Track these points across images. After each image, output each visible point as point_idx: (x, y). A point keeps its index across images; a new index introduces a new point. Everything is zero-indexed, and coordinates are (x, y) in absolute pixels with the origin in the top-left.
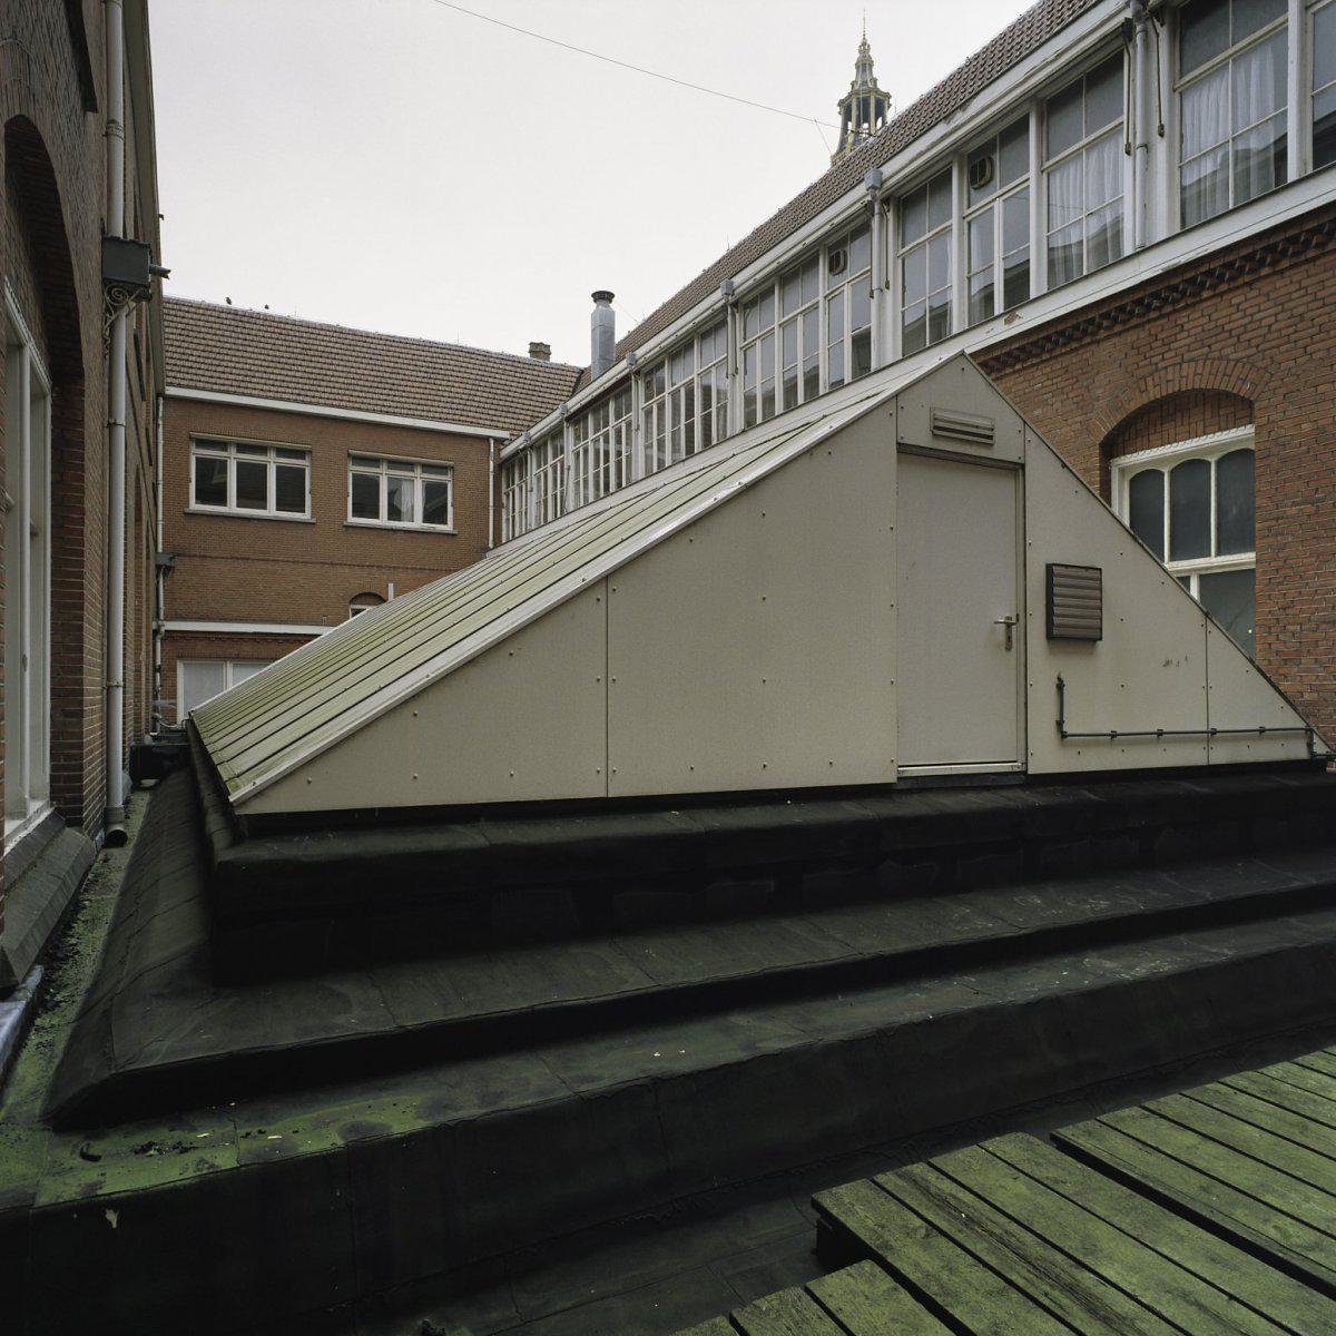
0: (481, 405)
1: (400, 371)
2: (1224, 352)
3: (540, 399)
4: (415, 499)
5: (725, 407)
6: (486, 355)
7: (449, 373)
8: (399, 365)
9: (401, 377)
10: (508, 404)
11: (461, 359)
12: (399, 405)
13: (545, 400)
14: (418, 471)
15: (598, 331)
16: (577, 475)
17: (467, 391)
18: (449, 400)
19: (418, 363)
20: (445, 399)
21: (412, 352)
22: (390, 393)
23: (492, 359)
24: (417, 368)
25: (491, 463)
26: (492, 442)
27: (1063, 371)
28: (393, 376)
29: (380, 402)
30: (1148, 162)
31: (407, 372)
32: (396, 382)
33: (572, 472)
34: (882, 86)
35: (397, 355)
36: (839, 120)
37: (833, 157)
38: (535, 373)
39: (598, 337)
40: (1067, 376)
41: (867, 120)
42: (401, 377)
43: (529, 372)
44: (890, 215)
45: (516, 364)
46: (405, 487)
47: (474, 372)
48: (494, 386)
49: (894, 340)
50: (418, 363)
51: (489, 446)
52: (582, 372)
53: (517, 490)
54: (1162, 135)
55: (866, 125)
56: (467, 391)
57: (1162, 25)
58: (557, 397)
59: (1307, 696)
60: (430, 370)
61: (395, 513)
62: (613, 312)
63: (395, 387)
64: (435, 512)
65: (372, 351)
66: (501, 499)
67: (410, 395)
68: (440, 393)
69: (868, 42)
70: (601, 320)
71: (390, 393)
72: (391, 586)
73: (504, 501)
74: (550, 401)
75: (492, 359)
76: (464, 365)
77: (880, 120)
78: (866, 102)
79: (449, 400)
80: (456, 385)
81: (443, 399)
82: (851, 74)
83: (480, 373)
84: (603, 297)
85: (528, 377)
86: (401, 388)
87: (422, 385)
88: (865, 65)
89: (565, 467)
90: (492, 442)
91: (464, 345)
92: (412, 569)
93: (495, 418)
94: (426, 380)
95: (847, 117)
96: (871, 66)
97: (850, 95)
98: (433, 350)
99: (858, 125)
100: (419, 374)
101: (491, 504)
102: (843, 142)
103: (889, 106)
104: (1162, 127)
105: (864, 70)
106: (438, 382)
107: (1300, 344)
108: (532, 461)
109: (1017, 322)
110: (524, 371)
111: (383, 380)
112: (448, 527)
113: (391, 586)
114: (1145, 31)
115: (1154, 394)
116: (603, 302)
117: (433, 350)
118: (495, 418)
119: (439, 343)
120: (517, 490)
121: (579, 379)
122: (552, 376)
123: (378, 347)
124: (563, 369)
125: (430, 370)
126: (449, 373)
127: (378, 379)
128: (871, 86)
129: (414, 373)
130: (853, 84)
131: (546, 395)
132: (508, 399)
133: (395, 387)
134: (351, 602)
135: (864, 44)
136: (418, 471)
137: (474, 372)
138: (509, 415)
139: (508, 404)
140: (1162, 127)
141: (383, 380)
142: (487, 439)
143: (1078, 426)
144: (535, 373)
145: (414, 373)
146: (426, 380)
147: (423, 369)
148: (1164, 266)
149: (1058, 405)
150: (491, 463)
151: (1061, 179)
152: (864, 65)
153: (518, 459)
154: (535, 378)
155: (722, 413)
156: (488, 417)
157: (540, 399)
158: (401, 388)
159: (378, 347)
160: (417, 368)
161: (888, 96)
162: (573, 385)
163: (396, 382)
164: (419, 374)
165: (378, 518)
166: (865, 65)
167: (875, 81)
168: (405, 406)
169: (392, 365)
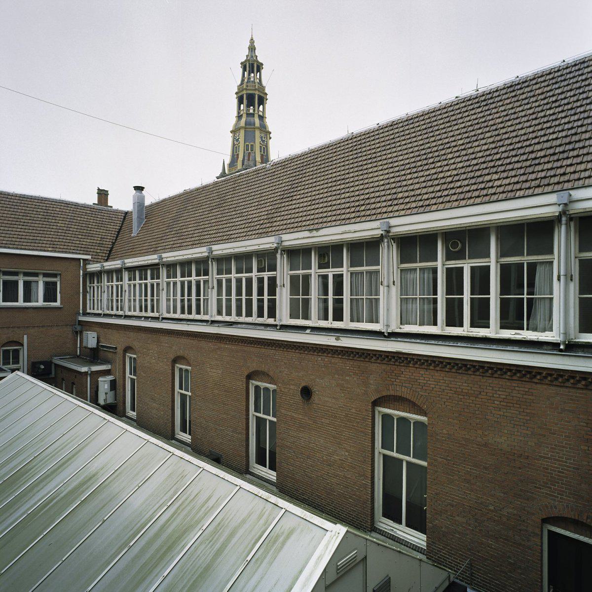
0: (74, 233)
1: (28, 215)
2: (417, 390)
3: (105, 228)
4: (40, 290)
5: (208, 299)
6: (76, 205)
7: (56, 215)
8: (27, 212)
9: (28, 218)
10: (88, 232)
11: (62, 207)
12: (28, 234)
13: (108, 229)
14: (41, 277)
15: (136, 205)
16: (130, 296)
17: (66, 225)
18: (56, 230)
19: (38, 210)
20: (54, 230)
21: (35, 203)
22: (23, 227)
23: (79, 207)
24: (38, 213)
25: (81, 272)
26: (82, 261)
27: (357, 367)
28: (24, 217)
29: (16, 233)
30: (389, 292)
31: (32, 215)
32: (26, 221)
33: (127, 293)
34: (260, 60)
35: (26, 205)
36: (241, 70)
37: (238, 86)
38: (102, 214)
39: (136, 207)
40: (359, 369)
41: (253, 72)
42: (28, 218)
43: (99, 214)
44: (285, 256)
45: (92, 210)
46: (33, 285)
47: (70, 214)
48: (81, 222)
49: (286, 310)
50: (38, 210)
51: (80, 264)
52: (126, 213)
53: (96, 288)
54: (394, 285)
55: (252, 75)
56: (66, 225)
57: (394, 242)
58: (114, 227)
59: (443, 529)
60: (45, 214)
61: (27, 299)
62: (144, 196)
63: (25, 224)
64: (50, 295)
65: (11, 203)
66: (86, 289)
67: (34, 228)
68: (51, 227)
69: (254, 39)
70: (138, 200)
71: (23, 227)
72: (25, 337)
73: (88, 290)
74: (111, 229)
75: (79, 207)
76: (64, 210)
77: (258, 73)
78: (252, 66)
79: (56, 230)
80: (60, 222)
81: (52, 230)
82: (246, 52)
83: (73, 215)
84: (139, 189)
85: (99, 216)
86: (29, 224)
87: (41, 222)
88: (252, 49)
89: (124, 290)
90: (82, 261)
91: (64, 199)
92: (37, 327)
93: (81, 240)
94: (43, 220)
95: (244, 70)
96: (255, 49)
97: (246, 61)
98: (46, 202)
99: (249, 75)
100: (39, 216)
101: (81, 291)
102: (243, 80)
103: (262, 68)
104: (394, 282)
105: (252, 51)
106: (50, 220)
107: (444, 400)
108: (105, 278)
109: (340, 341)
110: (97, 213)
111: (18, 220)
112: (58, 304)
113: (25, 337)
114: (388, 242)
115: (392, 393)
116: (138, 191)
117: (46, 202)
118: (81, 240)
119: (50, 199)
120: (96, 288)
121: (125, 217)
122: (111, 216)
123: (15, 201)
124: (117, 212)
125: (45, 214)
126: (56, 215)
127: (16, 220)
128: (255, 59)
129: (36, 216)
130: (247, 56)
131: (108, 226)
132: (88, 229)
133: (25, 224)
134: (1, 347)
135: (252, 40)
136: (41, 277)
137: (70, 214)
138: (89, 238)
139: (88, 232)
140: (394, 282)
141: (18, 220)
142: (79, 259)
143: (363, 392)
144: (102, 214)
145: (36, 216)
146: (43, 220)
147: (42, 213)
148: (397, 350)
149: (355, 379)
150: (81, 272)
151: (356, 277)
152: (252, 49)
153: (98, 275)
154: (102, 217)
155: (206, 302)
156: (78, 239)
157: (105, 228)
158: (29, 224)
159: (15, 201)
160: (38, 213)
161: (262, 64)
162: (122, 220)
163: (26, 221)
164: (39, 216)
165: (18, 302)
166: (252, 49)
167: (257, 57)
168: (32, 234)
169: (23, 211)
